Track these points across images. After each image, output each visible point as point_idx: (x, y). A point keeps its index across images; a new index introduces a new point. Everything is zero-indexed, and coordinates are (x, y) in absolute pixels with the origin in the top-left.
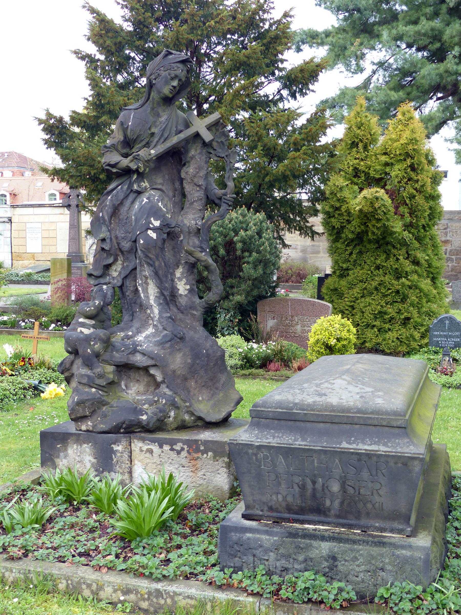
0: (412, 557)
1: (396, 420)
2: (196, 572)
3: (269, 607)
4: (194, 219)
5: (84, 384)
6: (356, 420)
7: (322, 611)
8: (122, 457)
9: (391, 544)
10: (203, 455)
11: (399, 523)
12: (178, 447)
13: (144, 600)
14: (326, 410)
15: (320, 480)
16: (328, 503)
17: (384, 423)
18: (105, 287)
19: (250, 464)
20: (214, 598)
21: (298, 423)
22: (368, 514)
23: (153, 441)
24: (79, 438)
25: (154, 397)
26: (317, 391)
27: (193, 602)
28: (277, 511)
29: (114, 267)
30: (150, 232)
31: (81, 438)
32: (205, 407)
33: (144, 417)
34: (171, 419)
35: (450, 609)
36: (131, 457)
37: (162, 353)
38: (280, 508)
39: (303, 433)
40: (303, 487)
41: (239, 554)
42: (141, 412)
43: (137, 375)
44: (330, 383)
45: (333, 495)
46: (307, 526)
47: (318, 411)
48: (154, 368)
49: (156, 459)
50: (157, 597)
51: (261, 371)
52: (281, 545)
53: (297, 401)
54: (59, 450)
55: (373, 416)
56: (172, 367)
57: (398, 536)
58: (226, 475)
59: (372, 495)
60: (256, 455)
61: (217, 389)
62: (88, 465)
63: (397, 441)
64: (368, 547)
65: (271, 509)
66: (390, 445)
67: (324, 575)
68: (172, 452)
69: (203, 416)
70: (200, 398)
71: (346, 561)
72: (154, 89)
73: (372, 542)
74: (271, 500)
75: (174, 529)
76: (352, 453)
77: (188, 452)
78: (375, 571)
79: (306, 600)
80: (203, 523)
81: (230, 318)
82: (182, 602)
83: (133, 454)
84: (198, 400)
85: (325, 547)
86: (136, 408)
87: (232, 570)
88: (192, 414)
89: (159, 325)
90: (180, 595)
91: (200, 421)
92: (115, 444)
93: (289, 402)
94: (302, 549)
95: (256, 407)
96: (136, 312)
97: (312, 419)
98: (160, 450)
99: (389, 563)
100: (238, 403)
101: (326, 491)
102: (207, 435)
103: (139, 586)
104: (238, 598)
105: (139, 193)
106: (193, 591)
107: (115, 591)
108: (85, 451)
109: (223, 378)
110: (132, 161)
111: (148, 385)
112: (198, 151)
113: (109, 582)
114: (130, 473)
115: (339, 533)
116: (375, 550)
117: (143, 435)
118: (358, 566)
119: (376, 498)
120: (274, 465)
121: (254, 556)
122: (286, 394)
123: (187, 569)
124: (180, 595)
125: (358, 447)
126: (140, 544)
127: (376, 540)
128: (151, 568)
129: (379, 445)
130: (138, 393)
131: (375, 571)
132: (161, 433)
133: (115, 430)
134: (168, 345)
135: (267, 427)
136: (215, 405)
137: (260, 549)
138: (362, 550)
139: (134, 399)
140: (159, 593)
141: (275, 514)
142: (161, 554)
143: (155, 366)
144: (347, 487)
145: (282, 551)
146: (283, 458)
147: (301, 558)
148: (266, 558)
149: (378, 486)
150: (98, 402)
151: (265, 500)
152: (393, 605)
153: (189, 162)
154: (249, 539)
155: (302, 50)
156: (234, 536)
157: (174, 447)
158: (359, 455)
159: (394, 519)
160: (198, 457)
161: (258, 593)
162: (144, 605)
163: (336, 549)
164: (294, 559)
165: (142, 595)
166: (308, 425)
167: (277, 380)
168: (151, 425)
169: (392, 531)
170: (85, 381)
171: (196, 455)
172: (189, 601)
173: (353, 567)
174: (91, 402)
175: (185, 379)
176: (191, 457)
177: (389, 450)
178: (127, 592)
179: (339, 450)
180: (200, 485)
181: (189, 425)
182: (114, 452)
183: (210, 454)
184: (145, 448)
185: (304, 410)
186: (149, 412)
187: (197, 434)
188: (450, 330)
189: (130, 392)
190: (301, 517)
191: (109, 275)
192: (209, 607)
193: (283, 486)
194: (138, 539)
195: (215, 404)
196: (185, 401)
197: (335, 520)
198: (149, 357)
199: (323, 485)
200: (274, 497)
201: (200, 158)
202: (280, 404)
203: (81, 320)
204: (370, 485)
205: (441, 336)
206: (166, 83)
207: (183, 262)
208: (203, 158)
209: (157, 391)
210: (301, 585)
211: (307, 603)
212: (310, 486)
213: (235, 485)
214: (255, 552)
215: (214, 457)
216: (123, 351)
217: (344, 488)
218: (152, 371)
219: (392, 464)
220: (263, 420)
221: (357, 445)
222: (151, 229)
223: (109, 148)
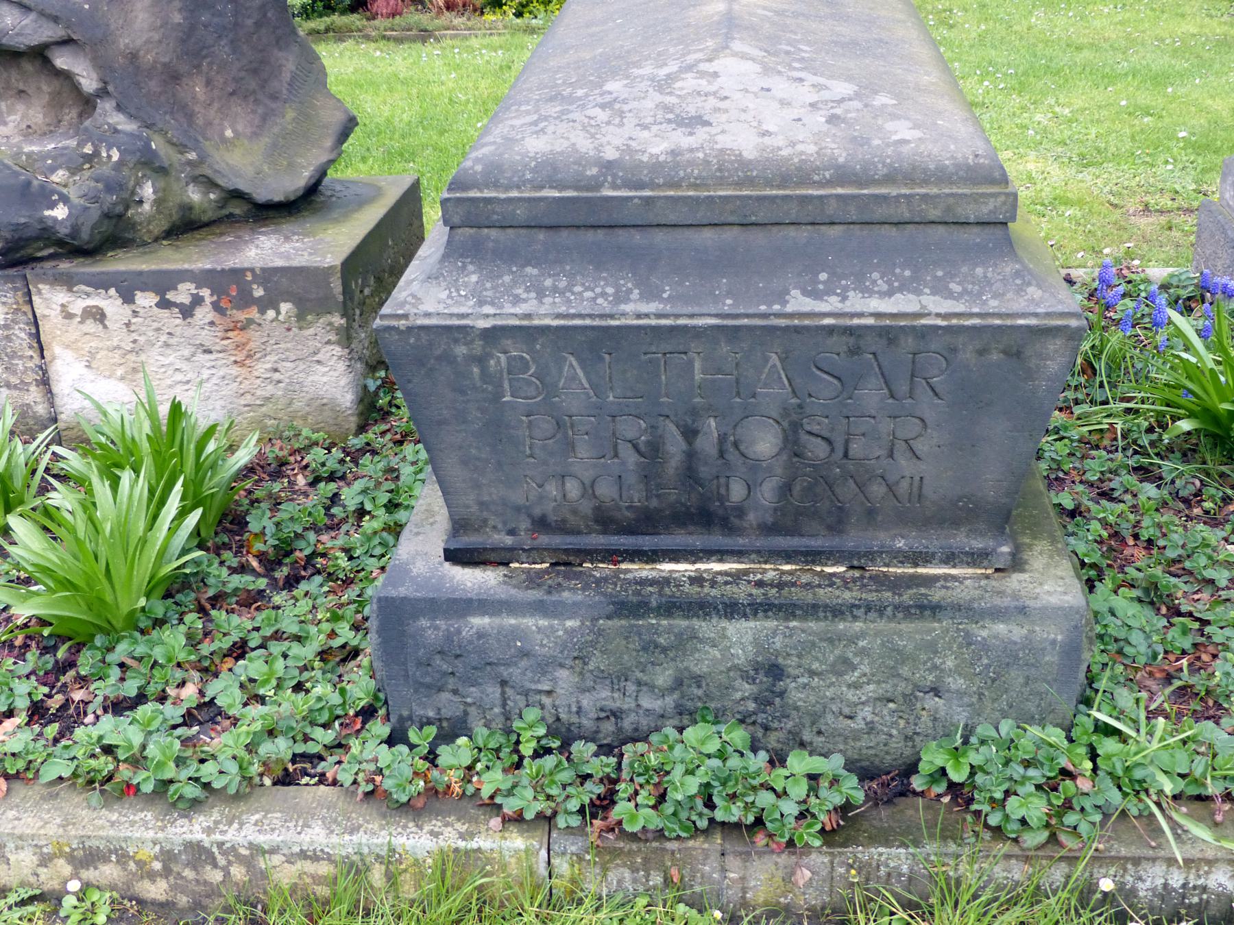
0: (1028, 644)
1: (976, 198)
2: (312, 748)
3: (581, 859)
6: (831, 209)
7: (760, 854)
9: (957, 608)
10: (262, 311)
11: (973, 532)
12: (182, 294)
13: (152, 876)
14: (721, 182)
15: (712, 422)
16: (737, 492)
17: (934, 214)
19: (463, 392)
20: (393, 851)
21: (622, 236)
22: (871, 513)
23: (100, 284)
25: (81, 144)
26: (668, 109)
27: (324, 869)
28: (562, 528)
32: (246, 157)
33: (60, 212)
34: (147, 207)
35: (1160, 792)
36: (37, 336)
38: (573, 520)
39: (643, 267)
40: (653, 451)
41: (451, 683)
42: (47, 196)
44: (702, 74)
45: (755, 467)
46: (667, 567)
47: (695, 186)
48: (65, 50)
49: (119, 336)
50: (194, 865)
51: (354, 19)
52: (593, 644)
53: (610, 154)
55: (893, 191)
56: (124, 42)
57: (970, 571)
58: (341, 366)
59: (891, 455)
60: (481, 360)
61: (274, 97)
63: (979, 271)
64: (882, 625)
65: (542, 524)
66: (955, 287)
67: (742, 721)
68: (165, 313)
69: (243, 186)
70: (229, 133)
71: (812, 673)
73: (896, 607)
74: (541, 498)
75: (211, 581)
76: (830, 330)
77: (216, 306)
78: (909, 699)
79: (703, 824)
80: (298, 536)
82: (285, 874)
83: (44, 327)
84: (224, 140)
85: (741, 637)
86: (28, 184)
87: (432, 731)
88: (211, 184)
90: (274, 851)
91: (236, 202)
93: (582, 161)
94: (664, 650)
95: (465, 188)
97: (672, 218)
98: (127, 310)
99: (958, 671)
100: (344, 135)
101: (732, 455)
102: (265, 250)
103: (126, 839)
104: (473, 845)
106: (316, 836)
107: (45, 861)
109: (289, 63)
111: (56, 104)
113: (20, 837)
114: (45, 382)
115: (780, 585)
116: (909, 633)
117: (64, 266)
118: (855, 686)
119: (905, 465)
120: (549, 388)
121: (504, 683)
122: (562, 128)
123: (281, 748)
124: (274, 851)
125: (848, 307)
126: (110, 658)
127: (907, 597)
128: (160, 765)
129: (918, 292)
130: (29, 132)
131: (909, 699)
132: (120, 253)
135: (511, 256)
136: (274, 152)
137: (524, 663)
138: (863, 635)
139: (19, 154)
140: (198, 854)
141: (557, 540)
142: (182, 684)
143: (67, 42)
144: (804, 437)
145: (597, 661)
146: (582, 363)
147: (663, 677)
148: (546, 688)
149: (910, 428)
151: (521, 501)
152: (986, 808)
154: (481, 635)
156: (431, 630)
157: (170, 296)
158: (852, 336)
159: (956, 523)
160: (250, 321)
161: (540, 816)
162: (156, 890)
163: (778, 642)
164: (639, 683)
165: (140, 864)
166: (659, 237)
167: (399, 41)
168: (85, 235)
169: (950, 559)
171: (241, 316)
172: (309, 867)
173: (840, 690)
175: (173, 77)
176: (228, 323)
177: (960, 308)
178: (88, 858)
179: (782, 322)
180: (267, 399)
181: (205, 218)
183: (285, 307)
185: (640, 186)
186: (73, 193)
187: (236, 247)
192: (377, 876)
193: (583, 451)
194: (99, 641)
195: (275, 145)
196: (182, 148)
197: (760, 542)
198: (42, 14)
199: (722, 439)
200: (552, 489)
202: (548, 171)
204: (886, 426)
209: (87, 123)
210: (684, 787)
211: (705, 832)
212: (675, 445)
213: (372, 388)
214: (505, 672)
215: (301, 317)
217: (796, 442)
218: (62, 61)
219: (967, 355)
220: (494, 233)
221: (844, 298)
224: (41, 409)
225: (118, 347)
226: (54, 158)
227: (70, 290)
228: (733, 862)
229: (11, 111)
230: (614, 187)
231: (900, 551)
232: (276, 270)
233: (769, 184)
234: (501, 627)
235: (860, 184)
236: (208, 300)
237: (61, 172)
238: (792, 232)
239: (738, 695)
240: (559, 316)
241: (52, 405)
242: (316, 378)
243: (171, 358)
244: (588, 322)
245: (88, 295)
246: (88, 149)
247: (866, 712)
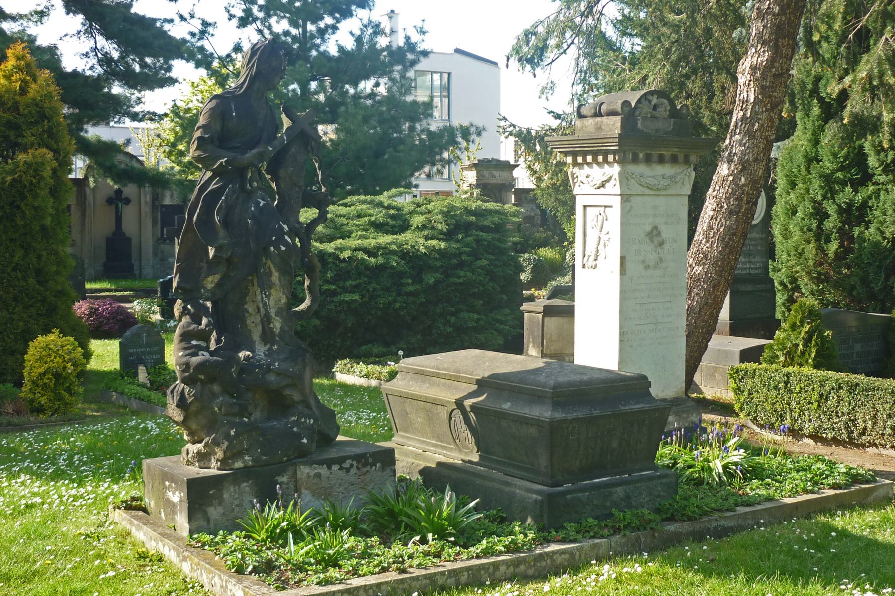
8: (287, 488)
12: (346, 465)
23: (320, 463)
77: (358, 468)
85: (620, 491)
98: (328, 473)
107: (508, 567)
155: (230, 19)
171: (365, 470)
183: (378, 465)
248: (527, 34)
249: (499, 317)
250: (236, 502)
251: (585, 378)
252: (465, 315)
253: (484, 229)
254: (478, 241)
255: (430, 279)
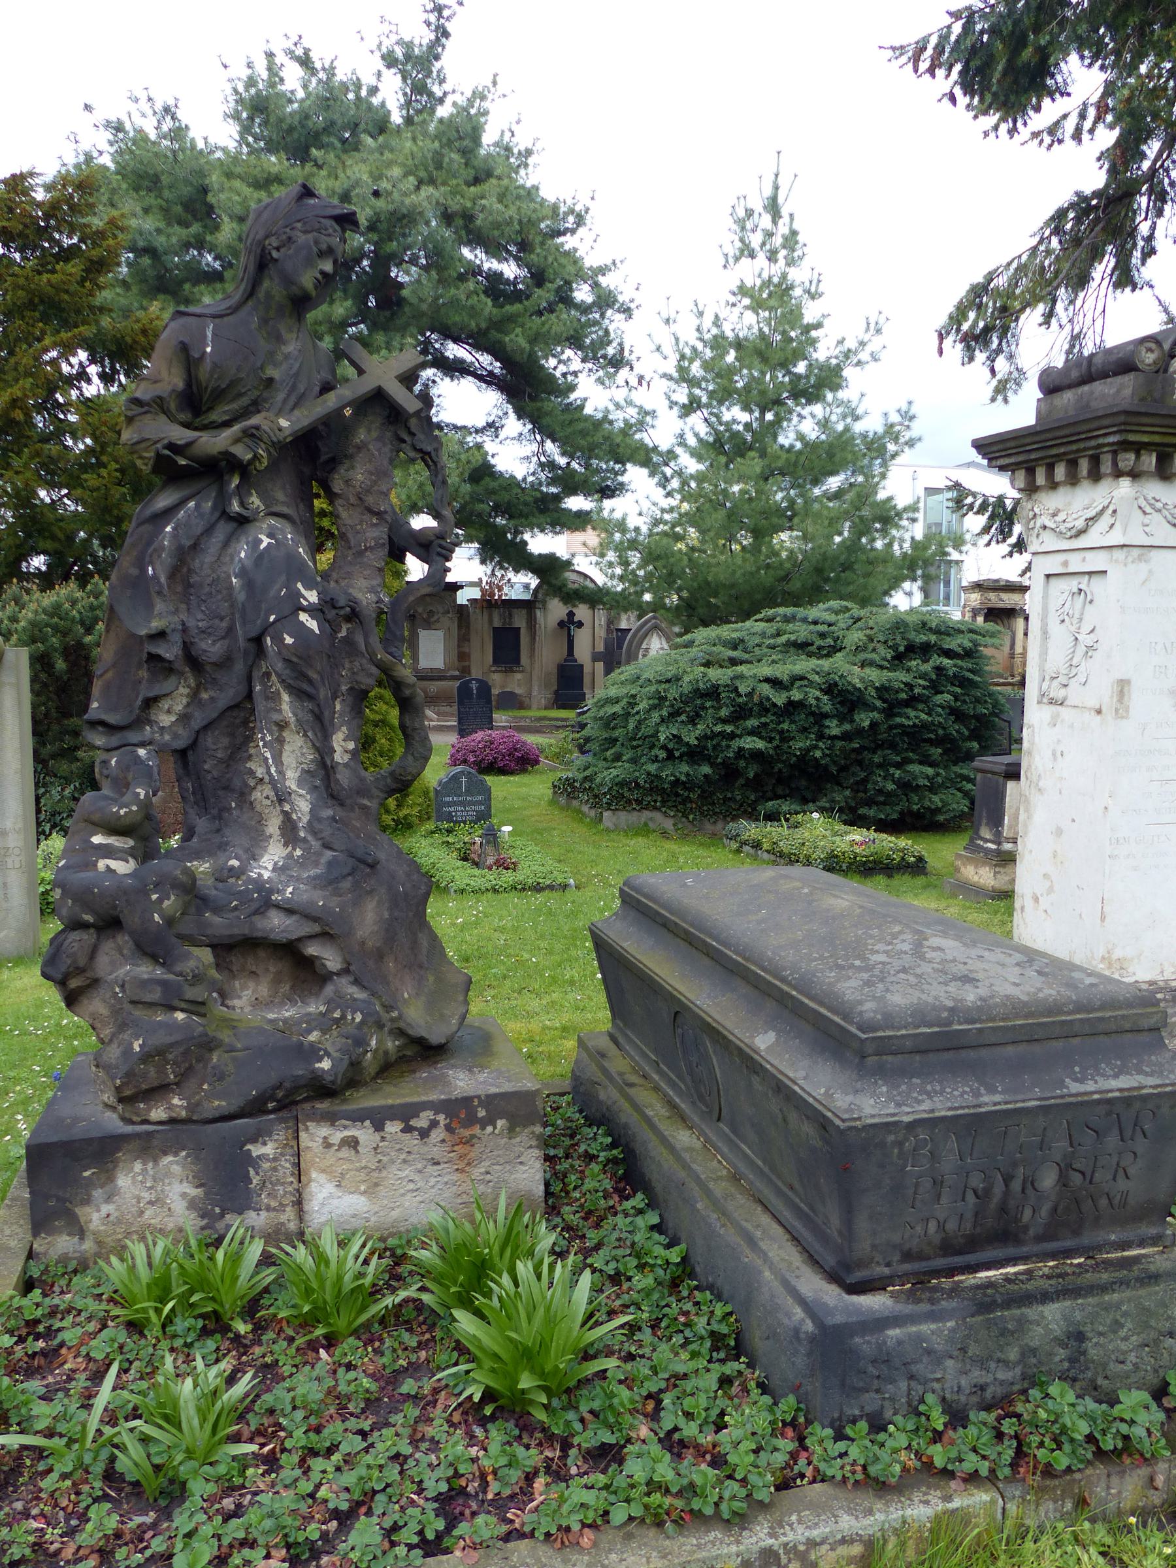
4: (372, 590)
5: (151, 1005)
10: (483, 1128)
12: (422, 1122)
14: (1017, 1016)
17: (1127, 1026)
18: (142, 752)
21: (964, 1054)
23: (357, 1117)
24: (148, 1145)
29: (165, 704)
30: (303, 617)
31: (155, 1142)
33: (326, 1064)
37: (335, 904)
42: (314, 1053)
43: (250, 960)
46: (983, 1274)
47: (1003, 1020)
49: (366, 1157)
52: (968, 1337)
54: (90, 1184)
59: (1114, 1179)
60: (900, 1144)
62: (180, 1207)
64: (1128, 1293)
65: (907, 1256)
71: (1100, 1334)
72: (272, 270)
76: (1099, 1102)
77: (448, 1128)
81: (72, 793)
83: (306, 1157)
85: (1052, 1317)
89: (310, 838)
90: (822, 1543)
92: (254, 1141)
96: (229, 809)
97: (994, 1040)
98: (377, 1136)
105: (242, 521)
108: (168, 1174)
110: (237, 441)
112: (374, 434)
114: (299, 1203)
116: (1148, 1296)
118: (1126, 1339)
130: (257, 1003)
131: (1157, 1342)
133: (255, 1108)
134: (347, 884)
135: (903, 1073)
147: (1013, 1354)
150: (200, 1046)
153: (351, 457)
154: (900, 1343)
160: (473, 1136)
164: (999, 1361)
166: (983, 1052)
169: (1141, 1244)
170: (155, 995)
171: (466, 1133)
174: (181, 1049)
182: (254, 1162)
183: (500, 1123)
184: (337, 1136)
188: (468, 792)
189: (236, 1003)
190: (971, 1258)
191: (150, 722)
197: (1037, 1248)
201: (379, 450)
202: (920, 1015)
203: (97, 839)
205: (455, 803)
206: (309, 262)
207: (344, 688)
208: (387, 449)
212: (998, 1189)
216: (236, 908)
220: (890, 1058)
222: (304, 610)
223: (148, 404)
224: (292, 1226)
225: (365, 1167)
226: (308, 1022)
227: (333, 1125)
228: (1115, 1480)
229: (243, 988)
230: (960, 1024)
231: (1115, 1242)
232: (496, 1095)
233: (1042, 1015)
234: (910, 1335)
235: (1089, 1012)
236: (442, 1123)
237: (315, 1033)
238: (1054, 1043)
239: (1057, 1359)
240: (950, 1109)
241: (301, 1219)
242: (517, 1176)
243: (407, 1172)
244: (966, 1111)
245: (345, 1127)
246: (337, 1015)
247: (1132, 1357)
248: (978, 292)
249: (965, 772)
250: (146, 1196)
251: (970, 996)
252: (915, 768)
253: (949, 654)
254: (939, 669)
255: (864, 719)
